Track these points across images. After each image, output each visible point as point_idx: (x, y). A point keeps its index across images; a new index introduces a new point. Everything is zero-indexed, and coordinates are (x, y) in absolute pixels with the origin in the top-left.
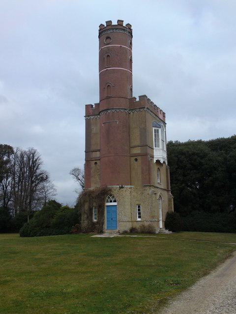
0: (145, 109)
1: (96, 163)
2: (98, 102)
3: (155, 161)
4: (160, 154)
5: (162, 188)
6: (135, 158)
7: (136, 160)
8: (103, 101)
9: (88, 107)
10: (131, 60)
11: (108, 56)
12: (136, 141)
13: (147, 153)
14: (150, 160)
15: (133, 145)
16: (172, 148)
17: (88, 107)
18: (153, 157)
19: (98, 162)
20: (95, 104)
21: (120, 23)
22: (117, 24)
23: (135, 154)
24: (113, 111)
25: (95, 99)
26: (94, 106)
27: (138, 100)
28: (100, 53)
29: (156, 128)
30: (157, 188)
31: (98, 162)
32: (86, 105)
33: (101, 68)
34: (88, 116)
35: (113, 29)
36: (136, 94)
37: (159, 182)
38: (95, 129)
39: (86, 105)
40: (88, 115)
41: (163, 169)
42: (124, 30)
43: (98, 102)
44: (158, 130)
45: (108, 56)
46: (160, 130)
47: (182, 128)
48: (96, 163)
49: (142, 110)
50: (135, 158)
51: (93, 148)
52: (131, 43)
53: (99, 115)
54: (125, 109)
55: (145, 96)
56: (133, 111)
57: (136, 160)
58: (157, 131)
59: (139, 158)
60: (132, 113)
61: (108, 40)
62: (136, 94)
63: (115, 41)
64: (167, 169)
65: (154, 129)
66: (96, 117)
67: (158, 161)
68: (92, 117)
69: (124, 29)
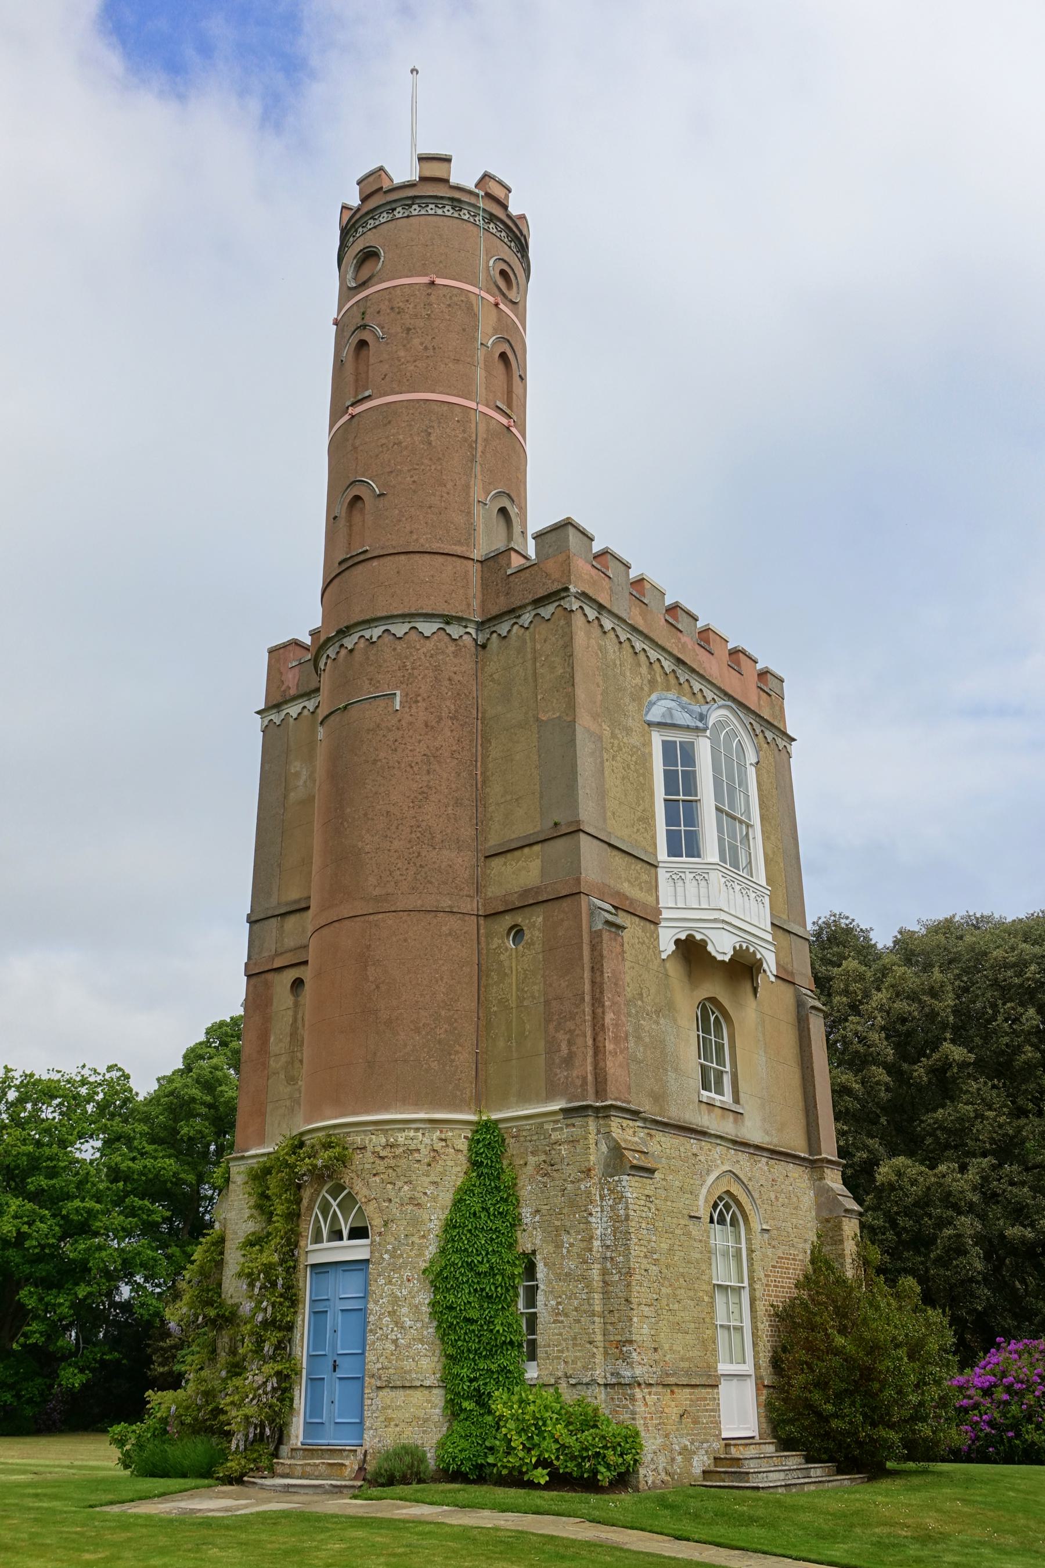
3: (667, 945)
5: (753, 1131)
6: (508, 920)
7: (517, 932)
18: (651, 919)
21: (435, 170)
29: (678, 737)
30: (701, 1133)
37: (727, 1098)
46: (703, 749)
48: (298, 984)
49: (546, 612)
56: (503, 628)
57: (517, 932)
67: (692, 952)
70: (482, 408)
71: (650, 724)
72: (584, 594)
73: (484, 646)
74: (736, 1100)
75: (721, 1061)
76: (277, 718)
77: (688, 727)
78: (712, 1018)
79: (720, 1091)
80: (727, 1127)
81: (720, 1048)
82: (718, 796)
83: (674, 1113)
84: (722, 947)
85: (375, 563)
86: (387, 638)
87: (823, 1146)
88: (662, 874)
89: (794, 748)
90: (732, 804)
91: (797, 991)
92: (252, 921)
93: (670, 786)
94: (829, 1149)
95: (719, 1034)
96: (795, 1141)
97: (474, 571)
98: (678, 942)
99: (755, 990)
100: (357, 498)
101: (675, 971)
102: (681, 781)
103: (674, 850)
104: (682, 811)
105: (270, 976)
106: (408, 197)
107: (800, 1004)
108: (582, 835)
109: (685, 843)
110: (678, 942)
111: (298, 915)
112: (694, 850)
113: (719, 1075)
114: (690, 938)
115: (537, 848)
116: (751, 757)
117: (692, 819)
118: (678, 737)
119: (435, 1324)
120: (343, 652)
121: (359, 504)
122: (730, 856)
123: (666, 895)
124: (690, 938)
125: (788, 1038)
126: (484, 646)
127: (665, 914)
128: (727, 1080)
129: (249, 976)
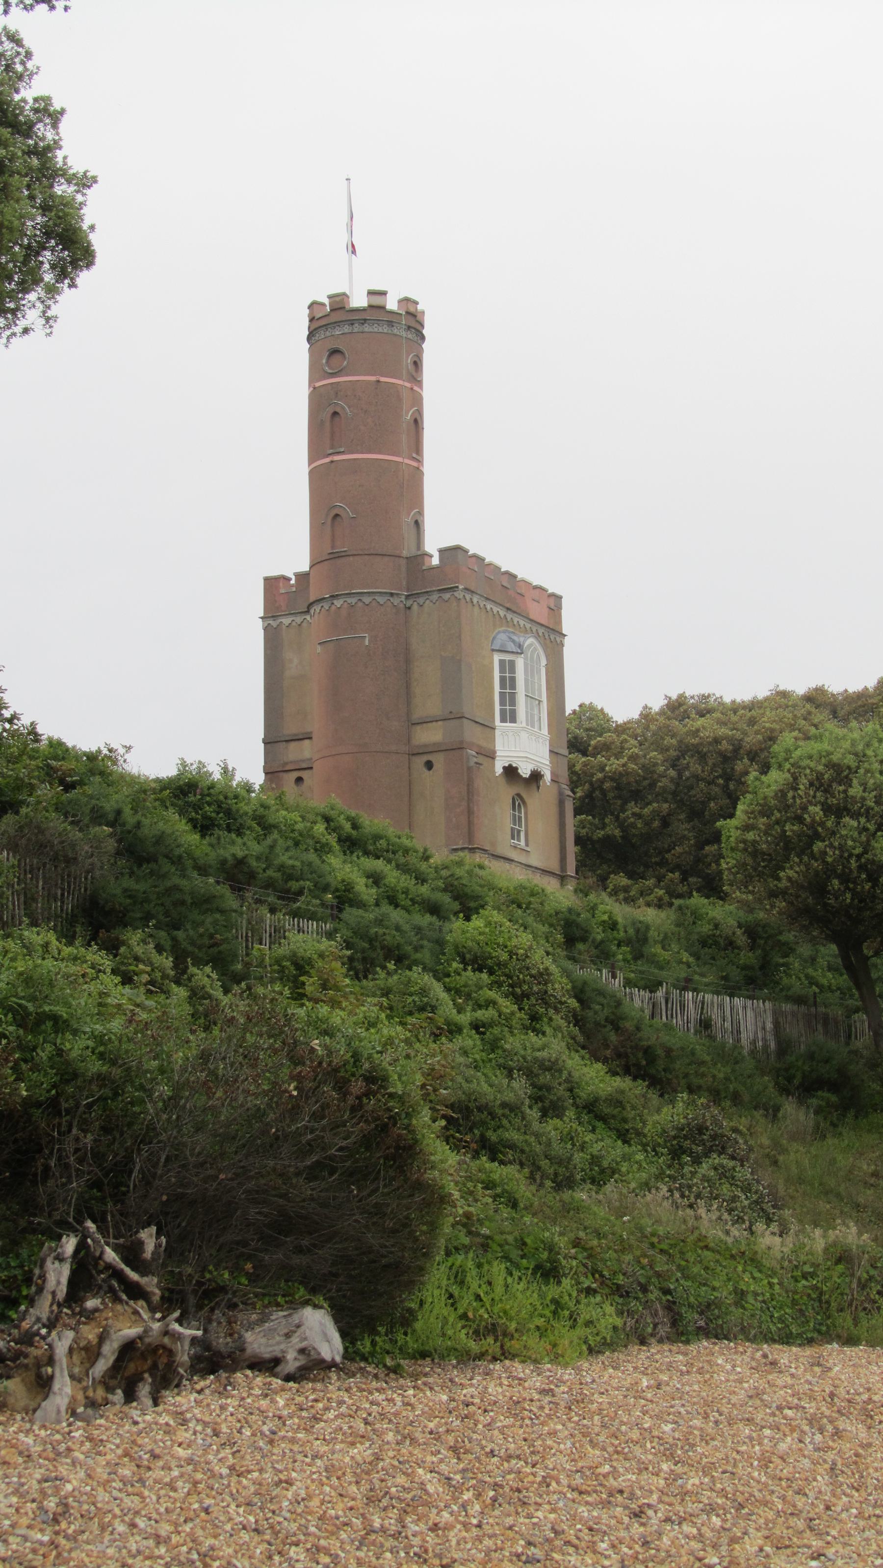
0: (459, 594)
1: (299, 780)
2: (305, 567)
3: (499, 770)
4: (524, 745)
5: (534, 861)
6: (426, 758)
7: (429, 765)
8: (321, 335)
9: (272, 584)
10: (417, 422)
11: (335, 414)
12: (428, 702)
13: (462, 742)
14: (472, 764)
15: (417, 715)
16: (583, 737)
17: (272, 584)
18: (491, 756)
19: (304, 774)
20: (297, 575)
21: (377, 301)
22: (366, 305)
23: (425, 746)
24: (353, 600)
25: (294, 557)
26: (293, 582)
27: (435, 561)
28: (311, 473)
29: (507, 657)
30: (510, 860)
31: (304, 774)
32: (266, 579)
33: (316, 449)
34: (274, 617)
35: (352, 323)
36: (435, 541)
37: (522, 843)
38: (293, 663)
39: (266, 579)
40: (272, 611)
41: (542, 812)
42: (390, 323)
43: (305, 567)
44: (512, 664)
45: (335, 414)
46: (520, 663)
47: (627, 668)
48: (299, 780)
49: (446, 596)
50: (426, 758)
51: (291, 728)
52: (417, 364)
53: (308, 612)
54: (392, 594)
55: (457, 549)
56: (421, 600)
57: (429, 765)
58: (508, 668)
59: (438, 760)
60: (415, 607)
61: (337, 358)
62: (435, 541)
63: (364, 368)
64: (561, 803)
65: (497, 658)
66: (299, 619)
67: (511, 772)
68: (286, 621)
69: (391, 319)
70: (407, 461)
71: (493, 650)
72: (466, 589)
73: (409, 608)
74: (527, 845)
75: (520, 826)
76: (274, 624)
77: (513, 652)
78: (518, 802)
79: (519, 840)
80: (522, 858)
81: (520, 818)
82: (527, 690)
83: (500, 851)
84: (525, 771)
85: (351, 558)
86: (360, 604)
87: (568, 868)
88: (498, 733)
89: (566, 641)
90: (534, 693)
91: (559, 787)
92: (266, 742)
93: (503, 685)
94: (571, 871)
95: (520, 812)
96: (555, 866)
97: (403, 562)
98: (504, 768)
99: (538, 788)
100: (337, 515)
101: (503, 781)
102: (509, 682)
103: (503, 720)
104: (509, 699)
105: (281, 774)
106: (359, 317)
107: (561, 794)
108: (465, 720)
109: (510, 716)
110: (504, 768)
111: (296, 743)
112: (513, 720)
113: (519, 832)
114: (510, 766)
115: (440, 723)
116: (544, 662)
117: (513, 702)
118: (507, 657)
119: (34, 1119)
120: (333, 607)
121: (338, 519)
122: (530, 722)
123: (499, 746)
124: (510, 766)
125: (554, 810)
126: (409, 608)
127: (498, 754)
128: (522, 835)
129: (266, 773)
